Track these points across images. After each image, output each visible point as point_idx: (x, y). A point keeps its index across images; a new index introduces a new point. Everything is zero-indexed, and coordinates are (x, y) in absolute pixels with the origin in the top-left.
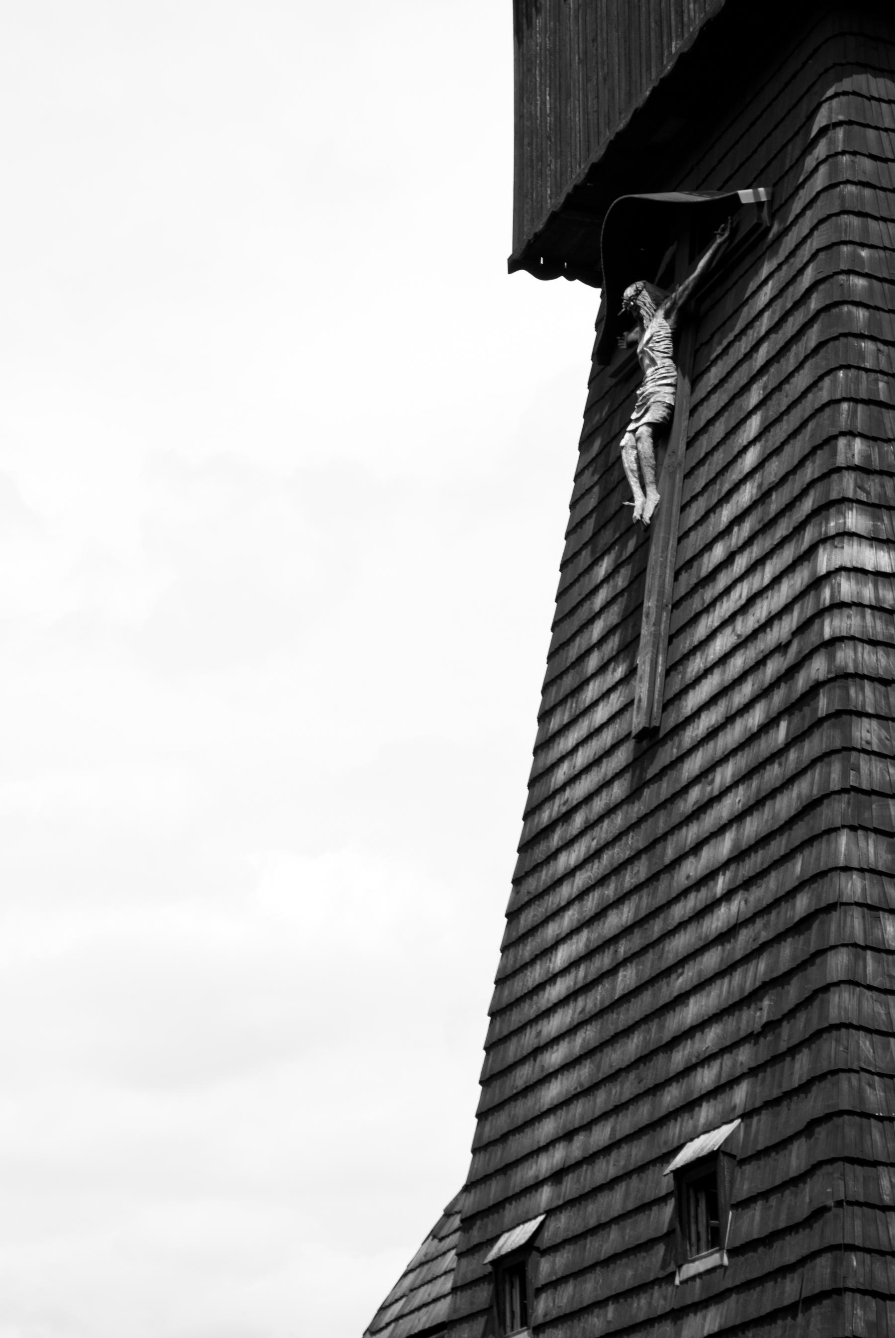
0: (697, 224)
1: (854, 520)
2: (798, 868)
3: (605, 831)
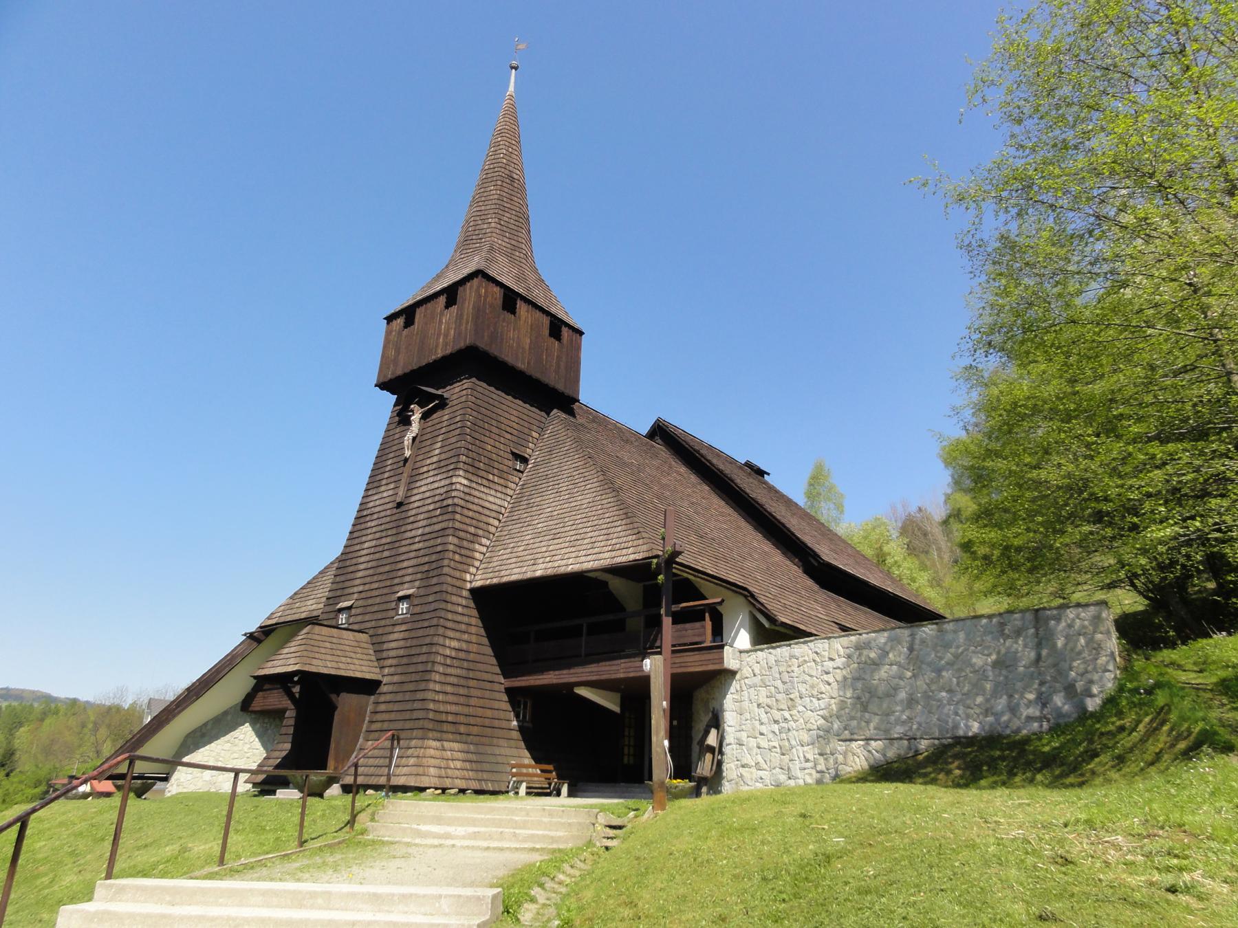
0: (433, 397)
1: (461, 473)
2: (439, 541)
3: (384, 520)
